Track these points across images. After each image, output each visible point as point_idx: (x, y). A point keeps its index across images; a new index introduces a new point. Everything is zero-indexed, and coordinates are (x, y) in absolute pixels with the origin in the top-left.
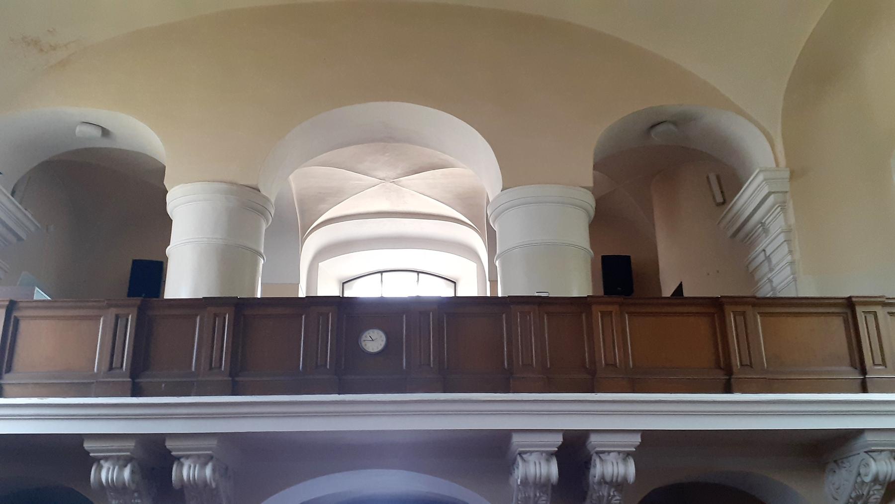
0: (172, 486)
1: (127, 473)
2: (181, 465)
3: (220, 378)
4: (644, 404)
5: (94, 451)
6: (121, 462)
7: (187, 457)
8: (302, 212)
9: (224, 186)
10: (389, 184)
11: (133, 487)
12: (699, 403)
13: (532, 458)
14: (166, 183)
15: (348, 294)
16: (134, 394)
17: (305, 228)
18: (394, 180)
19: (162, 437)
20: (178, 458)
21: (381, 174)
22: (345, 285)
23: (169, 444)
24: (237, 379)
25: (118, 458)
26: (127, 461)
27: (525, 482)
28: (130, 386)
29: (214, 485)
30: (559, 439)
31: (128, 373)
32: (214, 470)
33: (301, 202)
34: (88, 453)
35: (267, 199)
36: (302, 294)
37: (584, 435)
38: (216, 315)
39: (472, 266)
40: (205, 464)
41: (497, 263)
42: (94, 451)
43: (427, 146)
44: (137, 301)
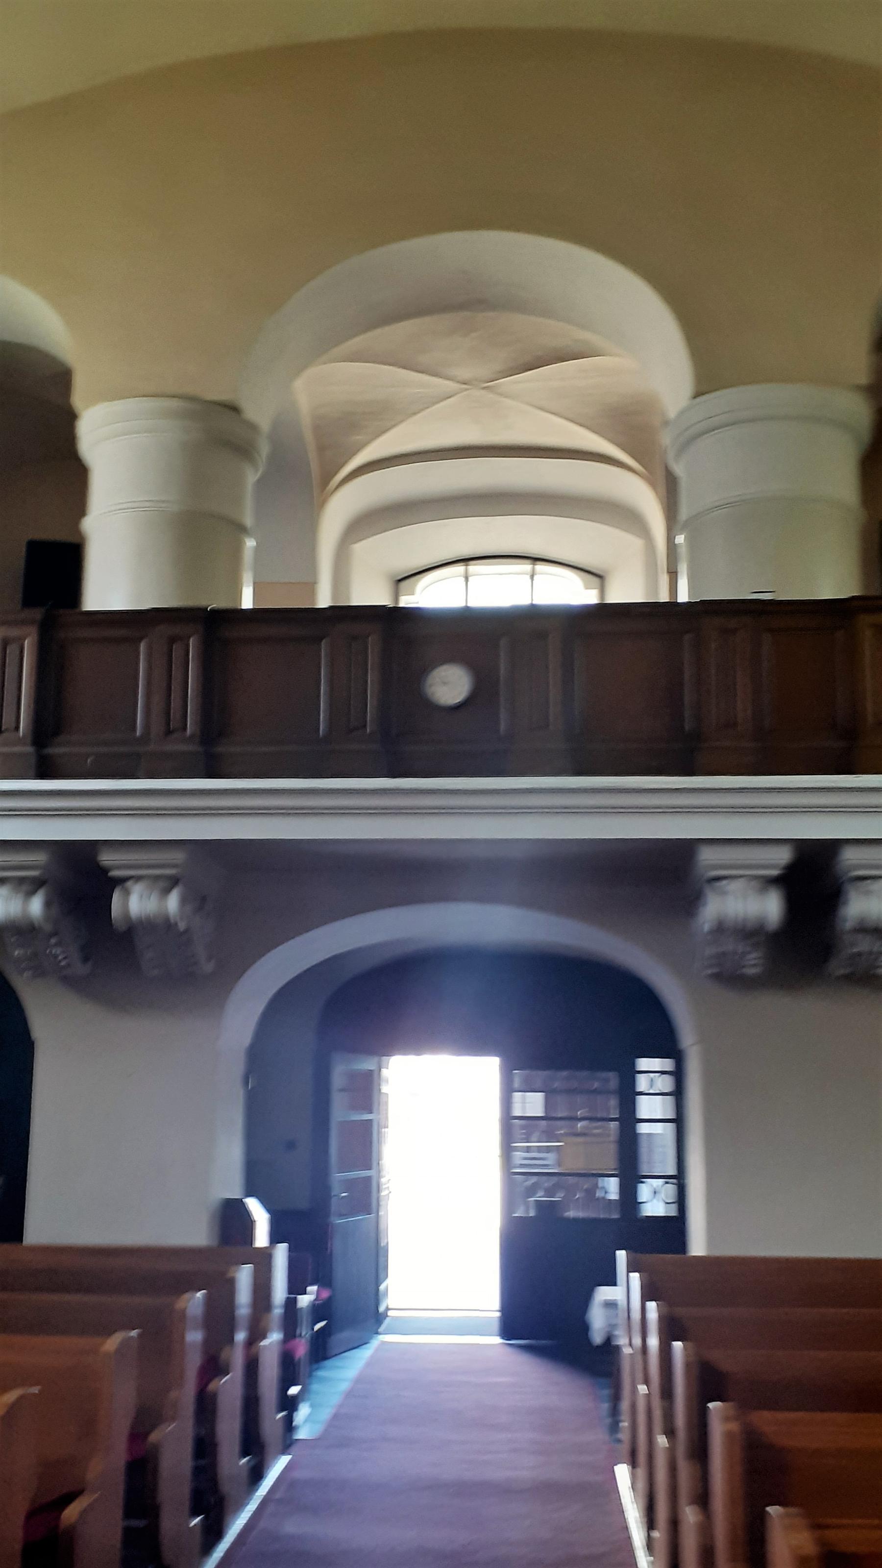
0: (111, 925)
1: (36, 906)
2: (127, 893)
3: (17, 749)
4: (623, 795)
5: (119, 867)
6: (162, 884)
7: (138, 879)
8: (321, 449)
9: (174, 403)
10: (477, 393)
11: (48, 928)
12: (648, 792)
13: (733, 886)
14: (77, 400)
15: (405, 602)
16: (42, 774)
17: (327, 478)
18: (487, 383)
19: (92, 847)
20: (122, 881)
21: (464, 373)
22: (404, 584)
23: (106, 858)
24: (220, 749)
25: (21, 880)
26: (34, 885)
27: (721, 929)
28: (33, 760)
29: (182, 926)
30: (783, 856)
31: (29, 740)
32: (183, 901)
33: (317, 429)
34: (104, 871)
35: (253, 427)
36: (324, 601)
37: (832, 847)
38: (172, 640)
39: (636, 543)
40: (167, 891)
41: (680, 539)
42: (119, 867)
43: (547, 312)
44: (37, 614)
